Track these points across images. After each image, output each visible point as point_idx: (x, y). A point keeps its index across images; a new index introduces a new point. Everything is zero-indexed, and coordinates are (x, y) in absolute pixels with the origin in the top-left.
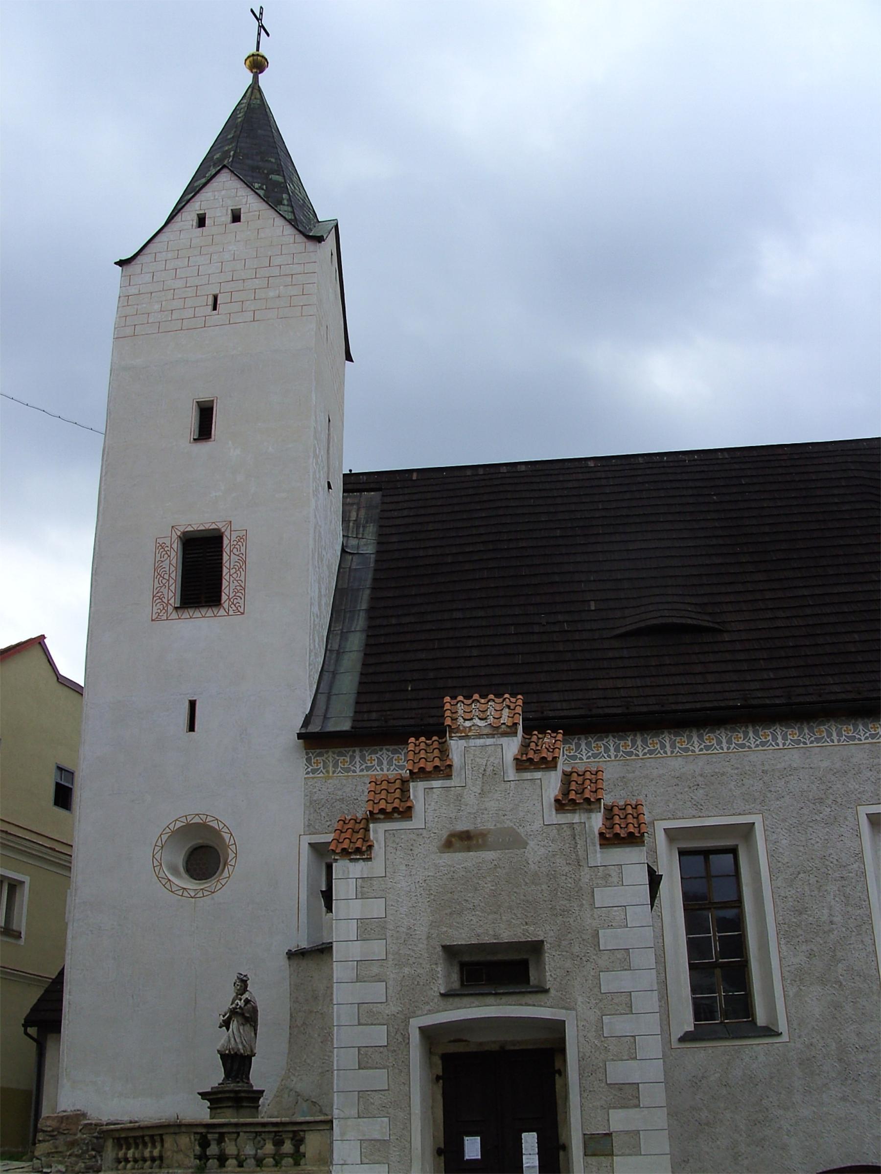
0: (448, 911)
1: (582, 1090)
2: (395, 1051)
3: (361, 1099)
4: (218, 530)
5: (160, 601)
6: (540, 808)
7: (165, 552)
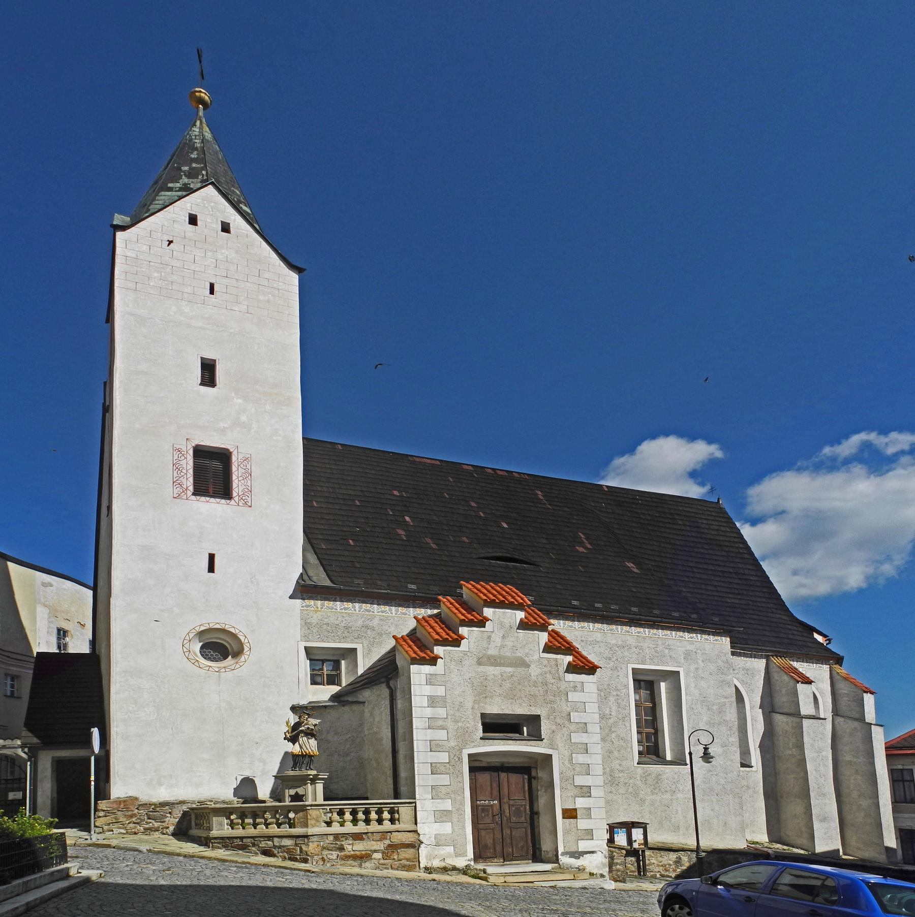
0: (484, 695)
1: (562, 788)
2: (454, 765)
3: (433, 790)
4: (228, 450)
5: (180, 486)
6: (538, 649)
7: (181, 455)
